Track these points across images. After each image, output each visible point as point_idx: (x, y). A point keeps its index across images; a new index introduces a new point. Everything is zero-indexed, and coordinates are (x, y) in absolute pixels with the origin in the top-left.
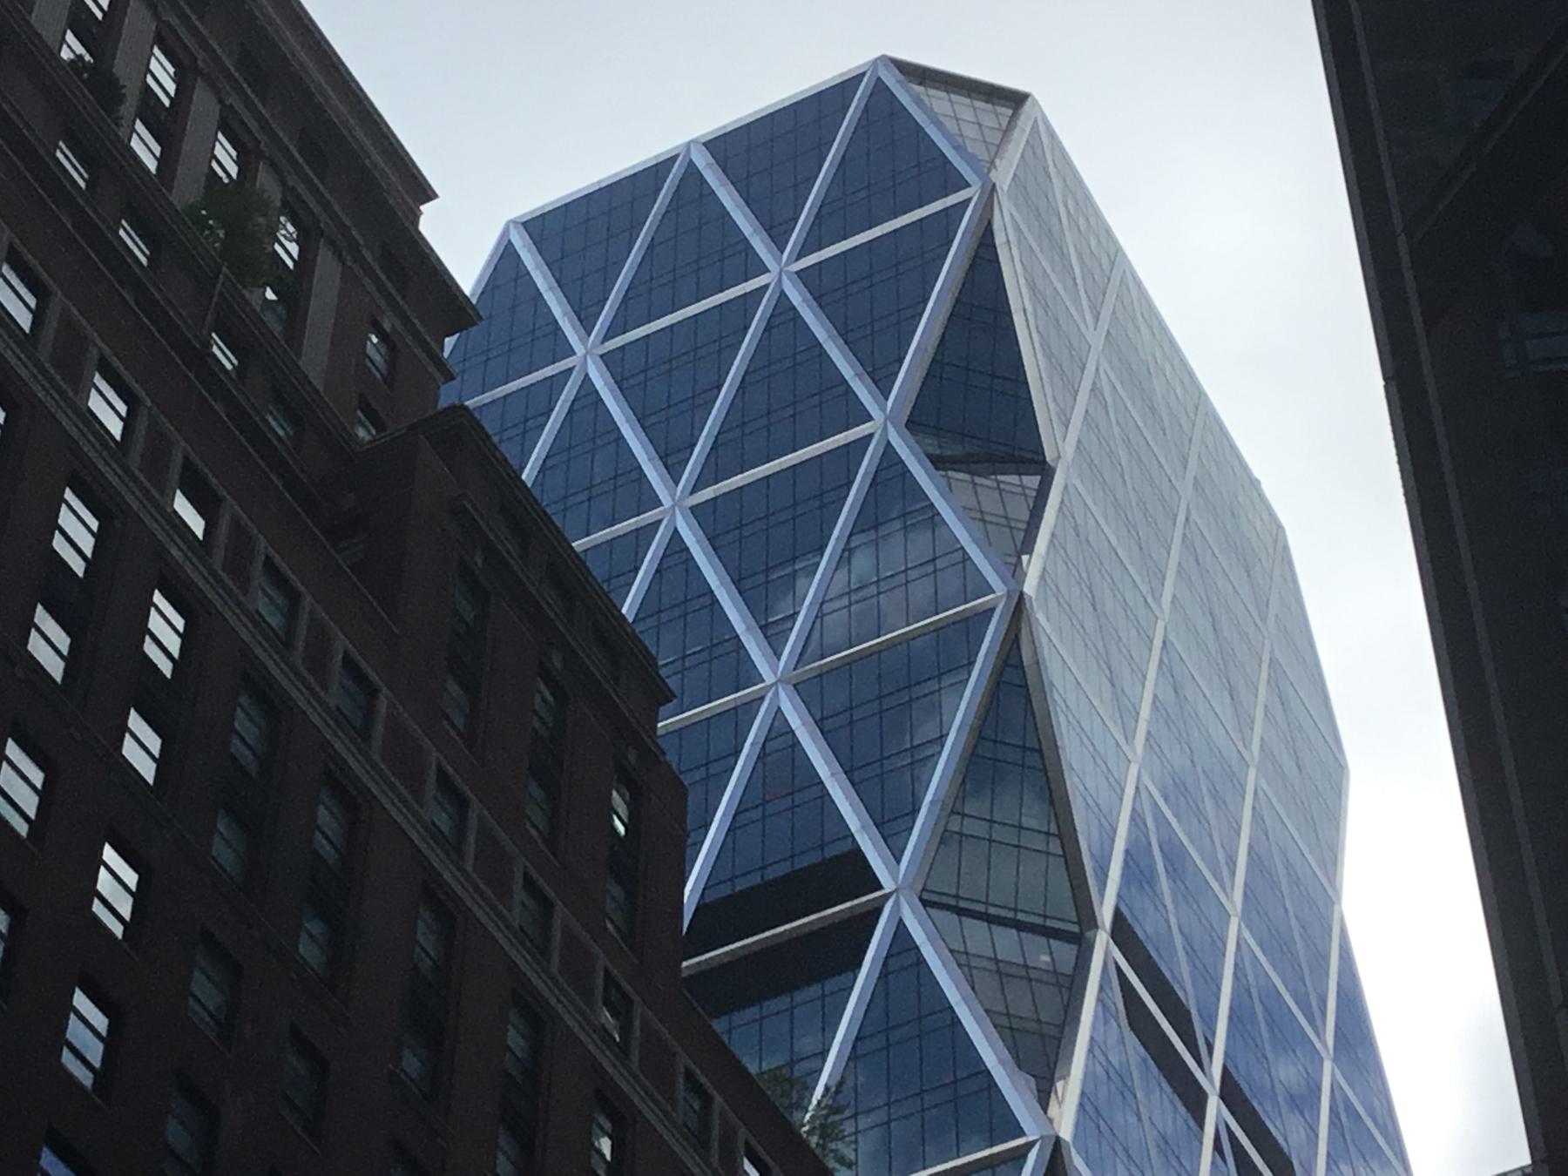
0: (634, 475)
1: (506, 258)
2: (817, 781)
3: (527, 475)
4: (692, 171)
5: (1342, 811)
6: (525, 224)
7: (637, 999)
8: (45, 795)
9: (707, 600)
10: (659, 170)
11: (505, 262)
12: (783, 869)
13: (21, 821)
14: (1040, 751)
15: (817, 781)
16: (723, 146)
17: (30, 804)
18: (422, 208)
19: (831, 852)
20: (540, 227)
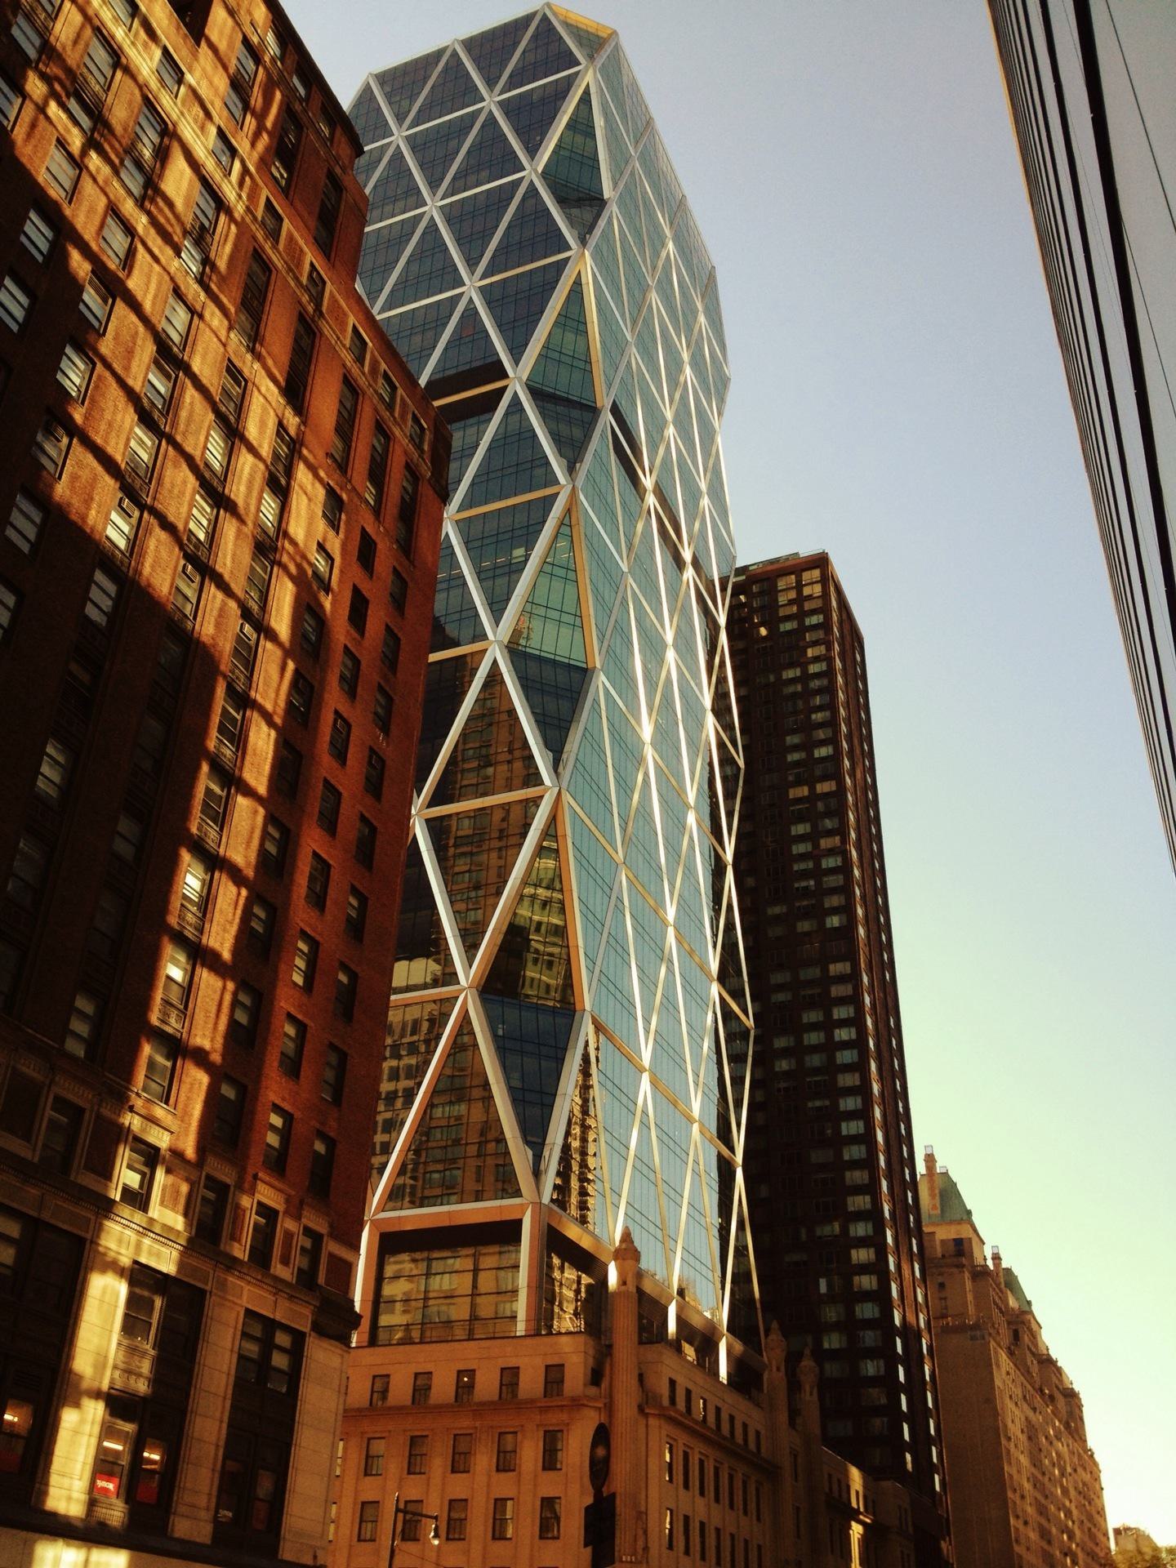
0: (543, 461)
1: (367, 91)
2: (407, 168)
3: (367, 191)
4: (455, 54)
5: (499, 942)
6: (376, 75)
7: (370, 344)
8: (29, 312)
9: (531, 434)
10: (439, 53)
11: (366, 96)
12: (478, 363)
13: (15, 324)
14: (570, 526)
15: (407, 168)
16: (470, 44)
17: (19, 314)
18: (1115, 1518)
19: (489, 360)
20: (383, 78)
